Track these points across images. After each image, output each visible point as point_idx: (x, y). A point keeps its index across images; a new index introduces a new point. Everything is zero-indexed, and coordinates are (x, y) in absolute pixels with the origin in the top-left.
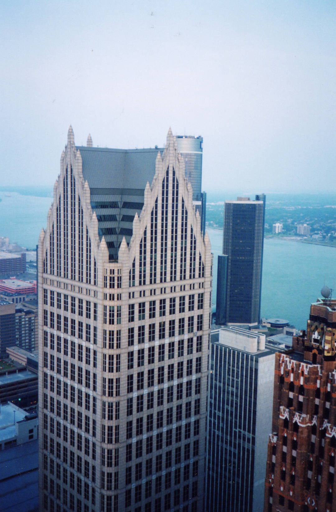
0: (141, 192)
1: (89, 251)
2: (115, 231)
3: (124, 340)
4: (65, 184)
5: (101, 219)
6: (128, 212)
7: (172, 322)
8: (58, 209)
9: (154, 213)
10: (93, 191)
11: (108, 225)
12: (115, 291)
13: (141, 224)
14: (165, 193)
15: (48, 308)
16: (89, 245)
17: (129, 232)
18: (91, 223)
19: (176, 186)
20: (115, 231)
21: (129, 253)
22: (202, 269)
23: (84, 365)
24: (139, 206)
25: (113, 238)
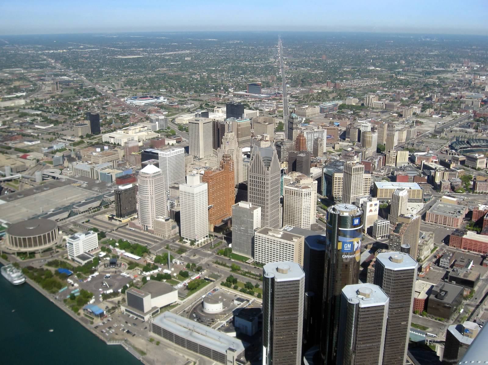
16: (263, 168)
18: (263, 164)
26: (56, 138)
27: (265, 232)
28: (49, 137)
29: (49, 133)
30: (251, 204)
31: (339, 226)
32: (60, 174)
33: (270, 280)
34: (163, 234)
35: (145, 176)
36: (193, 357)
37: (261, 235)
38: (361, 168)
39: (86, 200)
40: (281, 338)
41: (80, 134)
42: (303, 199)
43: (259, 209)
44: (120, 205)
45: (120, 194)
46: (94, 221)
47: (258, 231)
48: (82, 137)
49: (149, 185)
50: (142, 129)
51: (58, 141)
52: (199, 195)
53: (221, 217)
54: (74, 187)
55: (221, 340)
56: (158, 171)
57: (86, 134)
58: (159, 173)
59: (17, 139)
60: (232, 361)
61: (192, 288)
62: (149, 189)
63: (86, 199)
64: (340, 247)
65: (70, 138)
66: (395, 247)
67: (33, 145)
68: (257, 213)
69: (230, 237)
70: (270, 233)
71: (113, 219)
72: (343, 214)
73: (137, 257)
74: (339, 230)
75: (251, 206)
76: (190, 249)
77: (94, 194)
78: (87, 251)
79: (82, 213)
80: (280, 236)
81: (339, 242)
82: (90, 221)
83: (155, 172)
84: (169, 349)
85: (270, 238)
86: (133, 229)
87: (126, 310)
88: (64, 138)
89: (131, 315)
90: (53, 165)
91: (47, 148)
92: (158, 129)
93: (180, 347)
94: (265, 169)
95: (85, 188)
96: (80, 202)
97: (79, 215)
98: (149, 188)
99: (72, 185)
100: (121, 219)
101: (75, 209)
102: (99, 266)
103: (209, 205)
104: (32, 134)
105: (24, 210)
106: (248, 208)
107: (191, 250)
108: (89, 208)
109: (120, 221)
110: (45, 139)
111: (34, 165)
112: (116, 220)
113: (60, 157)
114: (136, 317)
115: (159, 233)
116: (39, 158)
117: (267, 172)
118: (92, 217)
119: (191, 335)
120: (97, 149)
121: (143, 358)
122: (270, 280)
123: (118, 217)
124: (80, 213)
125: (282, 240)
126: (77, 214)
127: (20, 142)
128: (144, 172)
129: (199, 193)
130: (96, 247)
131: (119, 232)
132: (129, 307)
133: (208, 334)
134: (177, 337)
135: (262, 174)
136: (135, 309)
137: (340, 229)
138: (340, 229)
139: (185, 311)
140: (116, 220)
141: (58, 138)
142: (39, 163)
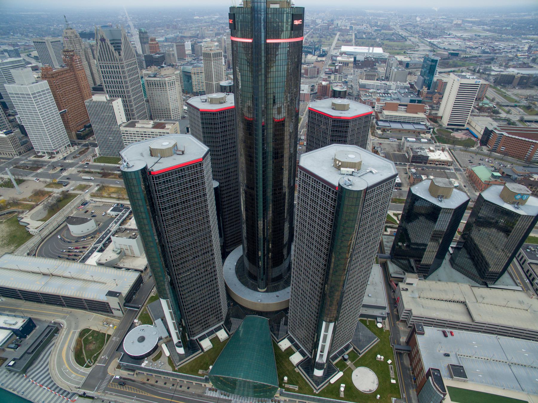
16: (113, 53)
18: (112, 48)
27: (133, 125)
30: (108, 96)
31: (266, 38)
34: (10, 153)
37: (127, 129)
43: (120, 100)
47: (124, 125)
53: (83, 123)
55: (280, 15)
60: (119, 308)
61: (53, 209)
68: (118, 105)
69: (363, 192)
70: (137, 125)
74: (267, 44)
75: (108, 98)
76: (49, 162)
80: (151, 126)
85: (138, 130)
94: (116, 54)
103: (60, 110)
105: (351, 156)
106: (105, 100)
107: (50, 164)
115: (5, 152)
125: (153, 130)
138: (268, 41)
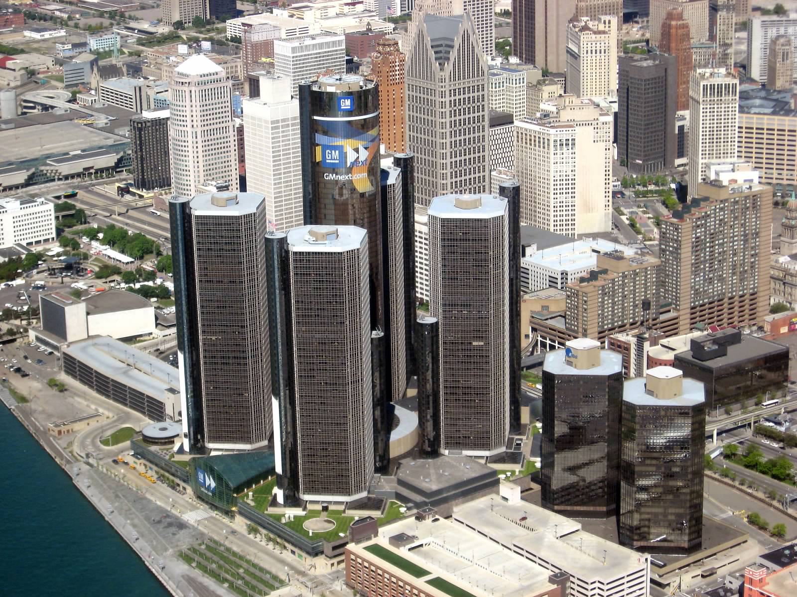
0: (453, 40)
1: (431, 67)
2: (442, 59)
3: (448, 146)
4: (419, 36)
5: (436, 53)
6: (448, 49)
7: (461, 181)
8: (415, 48)
9: (459, 50)
10: (432, 40)
11: (439, 55)
12: (443, 84)
13: (453, 55)
14: (463, 41)
15: (411, 93)
16: (431, 64)
17: (448, 59)
18: (431, 53)
19: (468, 37)
20: (442, 59)
21: (449, 67)
22: (483, 73)
23: (431, 178)
24: (452, 47)
25: (441, 61)
26: (112, 24)
28: (94, 22)
29: (101, 15)
32: (69, 101)
33: (178, 207)
35: (181, 80)
36: (108, 410)
38: (727, 86)
39: (83, 151)
40: (214, 338)
41: (176, 17)
42: (552, 156)
44: (142, 156)
45: (140, 130)
46: (89, 195)
48: (179, 25)
49: (188, 103)
50: (346, 9)
51: (64, 12)
52: (283, 127)
54: (78, 126)
56: (212, 71)
57: (192, 16)
58: (215, 77)
59: (12, 23)
62: (188, 114)
63: (84, 146)
64: (319, 158)
65: (146, 26)
66: (671, 252)
67: (44, 40)
71: (128, 192)
72: (326, 88)
73: (126, 259)
77: (108, 138)
78: (24, 243)
79: (66, 178)
81: (318, 145)
82: (78, 196)
83: (206, 72)
84: (78, 399)
86: (159, 213)
87: (38, 339)
88: (133, 24)
89: (43, 348)
90: (63, 85)
91: (70, 46)
92: (399, 13)
93: (103, 398)
95: (101, 129)
96: (67, 154)
97: (57, 183)
98: (188, 108)
99: (76, 121)
100: (144, 193)
101: (48, 168)
102: (35, 271)
104: (57, 13)
108: (85, 169)
109: (141, 197)
110: (81, 26)
111: (19, 83)
112: (134, 194)
113: (85, 63)
114: (50, 350)
116: (36, 68)
117: (439, 74)
118: (86, 188)
119: (125, 373)
120: (180, 46)
121: (16, 407)
122: (178, 207)
123: (138, 188)
124: (59, 179)
126: (53, 180)
127: (14, 31)
128: (181, 71)
129: (284, 120)
130: (50, 237)
131: (130, 218)
132: (47, 333)
133: (156, 373)
134: (99, 376)
135: (416, 77)
136: (54, 336)
137: (316, 118)
138: (316, 118)
139: (158, 350)
140: (134, 194)
141: (118, 24)
142: (33, 79)
